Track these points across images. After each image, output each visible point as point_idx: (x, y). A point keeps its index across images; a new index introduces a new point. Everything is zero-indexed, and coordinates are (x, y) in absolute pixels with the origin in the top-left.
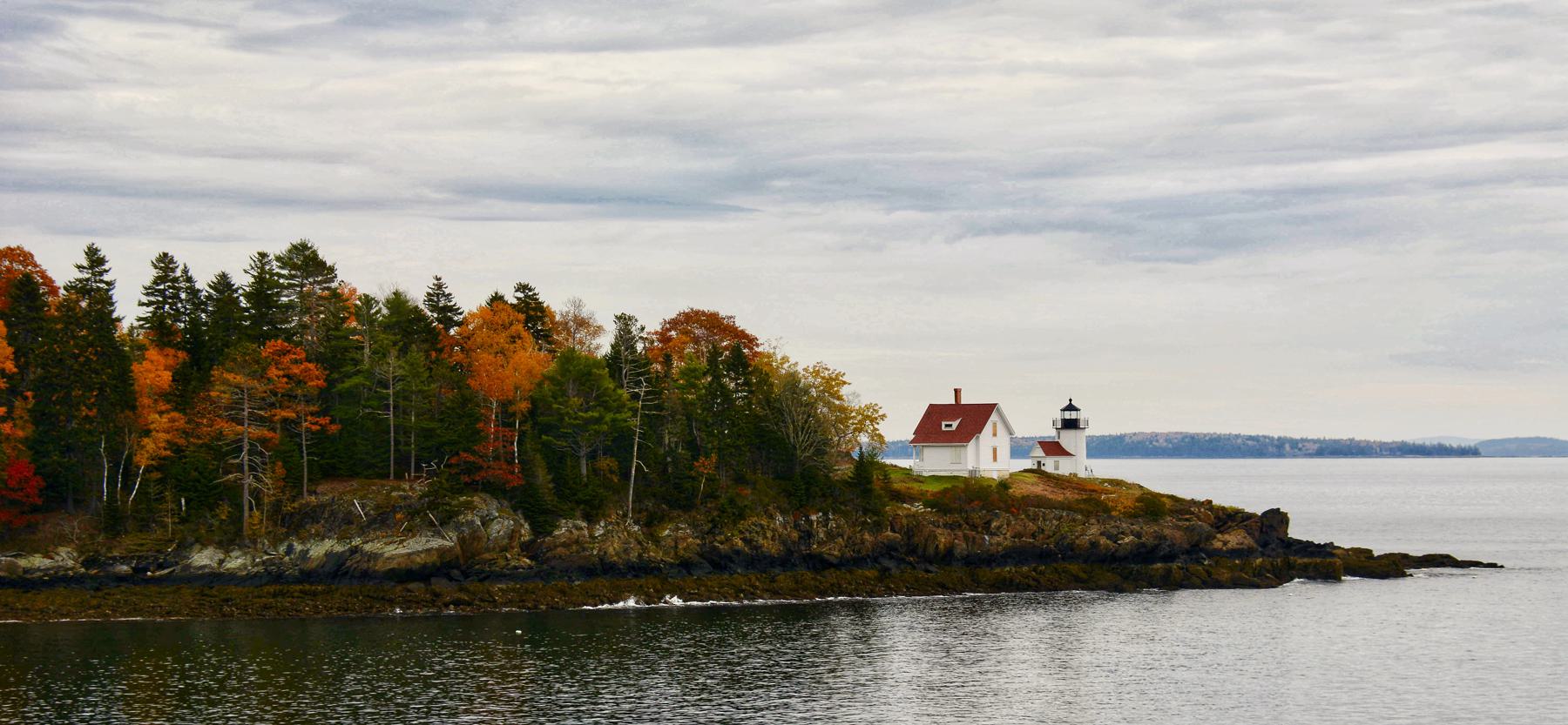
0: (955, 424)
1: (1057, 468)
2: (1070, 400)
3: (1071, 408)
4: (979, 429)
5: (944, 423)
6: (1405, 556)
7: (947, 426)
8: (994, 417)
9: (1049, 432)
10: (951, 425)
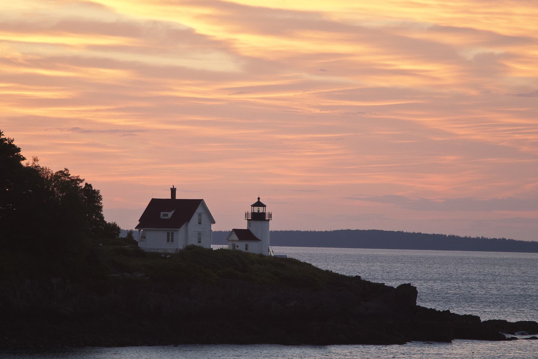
0: (170, 214)
1: (246, 249)
2: (259, 199)
3: (259, 204)
4: (188, 219)
5: (162, 213)
6: (503, 323)
7: (164, 215)
8: (199, 210)
9: (244, 225)
10: (167, 215)
